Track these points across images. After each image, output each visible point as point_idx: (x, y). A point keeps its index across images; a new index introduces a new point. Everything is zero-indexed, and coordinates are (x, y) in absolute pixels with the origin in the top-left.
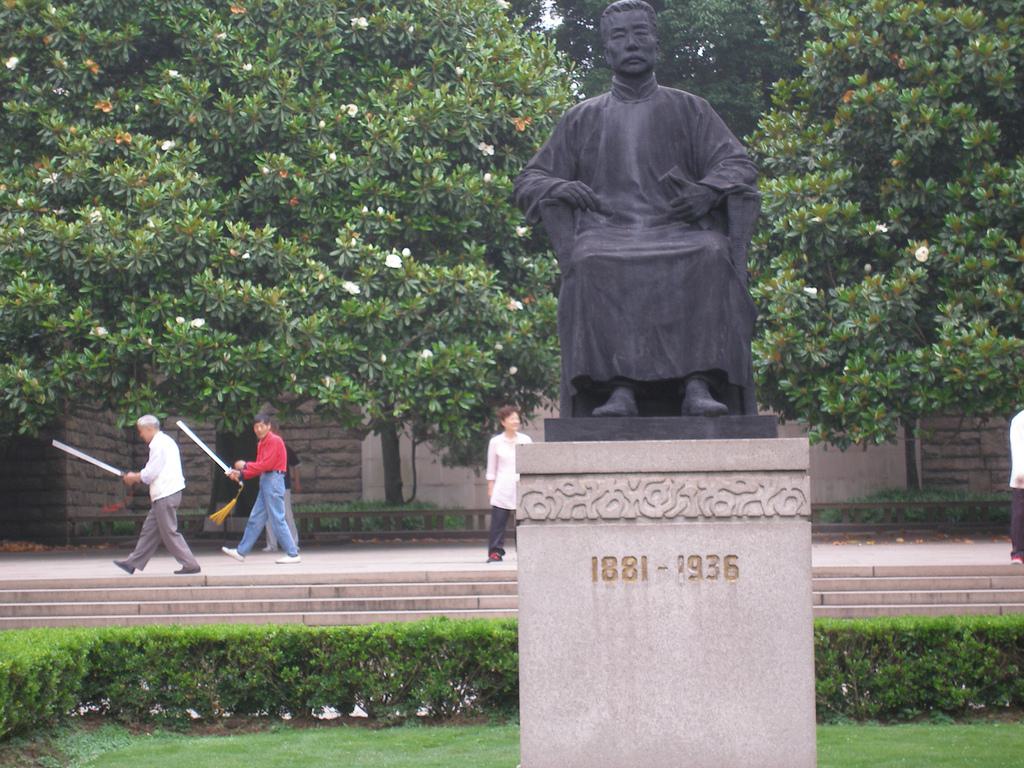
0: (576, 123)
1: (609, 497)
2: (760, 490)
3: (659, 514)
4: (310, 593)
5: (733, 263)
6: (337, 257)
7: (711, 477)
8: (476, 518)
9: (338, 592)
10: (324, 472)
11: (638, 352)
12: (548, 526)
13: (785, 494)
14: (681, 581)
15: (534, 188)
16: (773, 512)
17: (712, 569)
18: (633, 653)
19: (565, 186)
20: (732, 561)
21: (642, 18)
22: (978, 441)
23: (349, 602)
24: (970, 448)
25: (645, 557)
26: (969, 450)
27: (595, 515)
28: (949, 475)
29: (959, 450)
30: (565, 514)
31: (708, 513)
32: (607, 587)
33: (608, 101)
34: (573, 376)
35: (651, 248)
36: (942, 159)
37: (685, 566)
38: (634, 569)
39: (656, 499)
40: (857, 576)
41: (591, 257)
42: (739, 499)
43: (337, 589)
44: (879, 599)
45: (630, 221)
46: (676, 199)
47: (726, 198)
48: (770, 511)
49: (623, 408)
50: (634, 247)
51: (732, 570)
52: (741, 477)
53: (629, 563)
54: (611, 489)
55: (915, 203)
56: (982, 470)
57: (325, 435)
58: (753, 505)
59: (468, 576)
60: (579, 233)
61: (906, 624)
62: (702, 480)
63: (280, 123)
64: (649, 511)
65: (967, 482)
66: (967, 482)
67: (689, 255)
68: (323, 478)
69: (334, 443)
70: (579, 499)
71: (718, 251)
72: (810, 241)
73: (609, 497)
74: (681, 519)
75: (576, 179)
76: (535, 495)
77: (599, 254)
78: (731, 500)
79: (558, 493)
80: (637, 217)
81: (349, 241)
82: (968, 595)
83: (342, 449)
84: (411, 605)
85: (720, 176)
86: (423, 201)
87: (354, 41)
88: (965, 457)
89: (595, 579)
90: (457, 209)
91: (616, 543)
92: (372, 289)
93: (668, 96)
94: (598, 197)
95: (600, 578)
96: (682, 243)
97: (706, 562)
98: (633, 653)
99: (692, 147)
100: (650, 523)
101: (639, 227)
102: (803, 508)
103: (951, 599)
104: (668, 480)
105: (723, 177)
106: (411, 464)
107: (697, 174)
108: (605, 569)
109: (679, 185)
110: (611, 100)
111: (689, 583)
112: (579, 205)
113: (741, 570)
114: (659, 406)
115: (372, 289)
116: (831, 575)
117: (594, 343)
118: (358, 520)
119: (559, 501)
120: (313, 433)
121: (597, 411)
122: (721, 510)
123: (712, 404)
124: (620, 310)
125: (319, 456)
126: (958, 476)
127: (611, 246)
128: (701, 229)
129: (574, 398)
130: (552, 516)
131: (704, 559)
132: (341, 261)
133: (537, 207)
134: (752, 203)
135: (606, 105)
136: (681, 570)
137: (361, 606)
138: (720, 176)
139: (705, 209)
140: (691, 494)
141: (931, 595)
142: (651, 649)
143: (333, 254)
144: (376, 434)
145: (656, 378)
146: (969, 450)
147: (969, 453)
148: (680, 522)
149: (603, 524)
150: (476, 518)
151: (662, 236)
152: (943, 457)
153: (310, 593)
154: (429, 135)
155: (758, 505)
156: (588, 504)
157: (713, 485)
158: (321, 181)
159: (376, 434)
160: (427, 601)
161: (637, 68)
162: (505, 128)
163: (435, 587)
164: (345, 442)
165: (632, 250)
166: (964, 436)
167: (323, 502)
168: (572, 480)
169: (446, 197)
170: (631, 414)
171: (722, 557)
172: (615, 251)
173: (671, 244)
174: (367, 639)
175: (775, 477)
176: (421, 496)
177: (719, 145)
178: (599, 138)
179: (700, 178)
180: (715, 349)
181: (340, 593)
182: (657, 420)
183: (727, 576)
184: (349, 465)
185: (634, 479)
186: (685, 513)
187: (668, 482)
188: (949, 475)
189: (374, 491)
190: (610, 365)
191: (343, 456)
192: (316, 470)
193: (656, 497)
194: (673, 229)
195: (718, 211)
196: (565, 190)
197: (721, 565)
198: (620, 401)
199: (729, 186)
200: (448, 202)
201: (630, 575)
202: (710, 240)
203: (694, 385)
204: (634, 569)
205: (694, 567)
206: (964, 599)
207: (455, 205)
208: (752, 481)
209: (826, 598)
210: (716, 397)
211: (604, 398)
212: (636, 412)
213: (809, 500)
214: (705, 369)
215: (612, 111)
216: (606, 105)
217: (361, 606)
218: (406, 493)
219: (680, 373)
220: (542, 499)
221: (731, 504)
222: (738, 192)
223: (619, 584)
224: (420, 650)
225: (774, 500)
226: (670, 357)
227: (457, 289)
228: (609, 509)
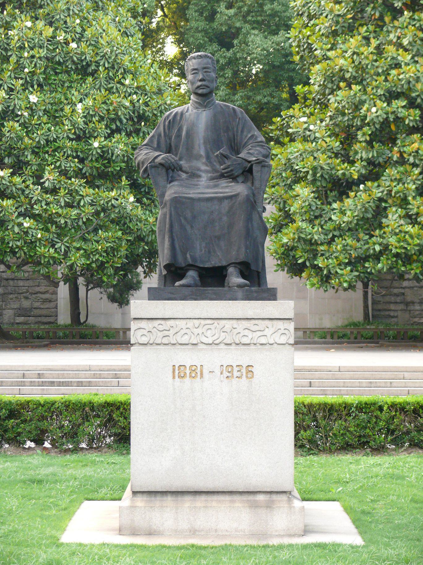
0: (170, 121)
1: (183, 332)
2: (267, 329)
3: (211, 342)
4: (23, 377)
5: (255, 202)
6: (44, 182)
7: (239, 322)
8: (121, 333)
9: (39, 376)
10: (36, 305)
11: (201, 251)
12: (149, 347)
14: (222, 379)
15: (145, 157)
16: (274, 342)
17: (239, 373)
18: (194, 419)
19: (162, 157)
20: (250, 369)
21: (208, 63)
22: (403, 294)
23: (45, 382)
24: (399, 298)
26: (398, 299)
27: (175, 342)
28: (387, 313)
29: (393, 299)
31: (238, 342)
32: (181, 382)
33: (188, 109)
34: (164, 264)
35: (210, 193)
36: (386, 133)
37: (224, 371)
38: (196, 372)
39: (209, 333)
40: (330, 371)
41: (176, 197)
43: (39, 374)
44: (342, 385)
46: (224, 165)
47: (252, 166)
49: (192, 282)
50: (200, 191)
51: (251, 373)
53: (193, 369)
54: (184, 328)
55: (370, 156)
56: (405, 310)
57: (37, 284)
59: (113, 368)
60: (170, 183)
61: (350, 399)
63: (15, 105)
64: (205, 340)
65: (397, 317)
66: (397, 317)
67: (231, 197)
69: (42, 289)
70: (166, 333)
71: (247, 195)
72: (314, 174)
73: (183, 332)
75: (169, 153)
76: (142, 330)
77: (181, 195)
79: (155, 329)
80: (203, 175)
81: (50, 177)
82: (391, 383)
84: (80, 384)
85: (249, 153)
86: (94, 153)
87: (57, 60)
89: (174, 377)
90: (114, 158)
91: (187, 358)
92: (65, 201)
93: (221, 107)
94: (181, 162)
96: (227, 190)
97: (236, 369)
98: (194, 419)
99: (234, 136)
102: (290, 340)
103: (381, 385)
104: (216, 322)
105: (249, 154)
106: (85, 301)
107: (238, 152)
108: (179, 372)
110: (190, 109)
111: (226, 381)
112: (170, 168)
114: (211, 281)
115: (65, 201)
116: (320, 371)
117: (177, 246)
118: (55, 333)
119: (155, 334)
120: (30, 283)
121: (177, 284)
122: (245, 340)
123: (241, 280)
124: (192, 227)
125: (34, 296)
126: (392, 314)
127: (187, 191)
128: (238, 182)
129: (165, 275)
130: (151, 342)
131: (235, 367)
132: (46, 185)
133: (147, 167)
134: (266, 169)
135: (187, 112)
136: (221, 373)
137: (52, 384)
138: (249, 153)
139: (241, 171)
140: (229, 331)
141: (370, 382)
143: (42, 181)
144: (65, 284)
145: (211, 266)
146: (398, 299)
147: (398, 301)
148: (222, 346)
149: (179, 347)
150: (121, 333)
151: (216, 186)
152: (384, 302)
153: (24, 376)
154: (99, 114)
155: (265, 337)
156: (171, 336)
157: (241, 326)
158: (37, 140)
159: (65, 284)
160: (90, 381)
162: (141, 112)
163: (94, 374)
164: (48, 288)
165: (199, 193)
166: (396, 291)
167: (36, 323)
169: (108, 151)
170: (197, 286)
171: (244, 366)
172: (189, 194)
173: (221, 190)
174: (52, 406)
175: (275, 322)
176: (91, 321)
177: (249, 135)
178: (182, 129)
179: (239, 154)
180: (244, 250)
181: (41, 378)
182: (210, 290)
183: (247, 377)
184: (50, 301)
185: (197, 322)
186: (224, 342)
187: (216, 324)
188: (387, 313)
189: (64, 317)
190: (186, 259)
191: (47, 296)
192: (32, 304)
193: (209, 331)
194: (223, 183)
195: (247, 172)
196: (163, 159)
197: (244, 371)
198: (192, 276)
199: (254, 159)
200: (108, 154)
201: (193, 375)
202: (240, 189)
203: (231, 270)
204: (196, 372)
205: (229, 371)
206: (389, 385)
207: (112, 156)
209: (312, 383)
210: (244, 276)
211: (181, 276)
212: (200, 284)
213: (293, 335)
214: (238, 261)
215: (190, 115)
216: (187, 112)
217: (52, 384)
218: (82, 320)
219: (224, 263)
220: (145, 332)
221: (250, 337)
222: (259, 162)
223: (187, 380)
224: (85, 411)
225: (274, 335)
226: (219, 254)
227: (113, 202)
228: (182, 339)
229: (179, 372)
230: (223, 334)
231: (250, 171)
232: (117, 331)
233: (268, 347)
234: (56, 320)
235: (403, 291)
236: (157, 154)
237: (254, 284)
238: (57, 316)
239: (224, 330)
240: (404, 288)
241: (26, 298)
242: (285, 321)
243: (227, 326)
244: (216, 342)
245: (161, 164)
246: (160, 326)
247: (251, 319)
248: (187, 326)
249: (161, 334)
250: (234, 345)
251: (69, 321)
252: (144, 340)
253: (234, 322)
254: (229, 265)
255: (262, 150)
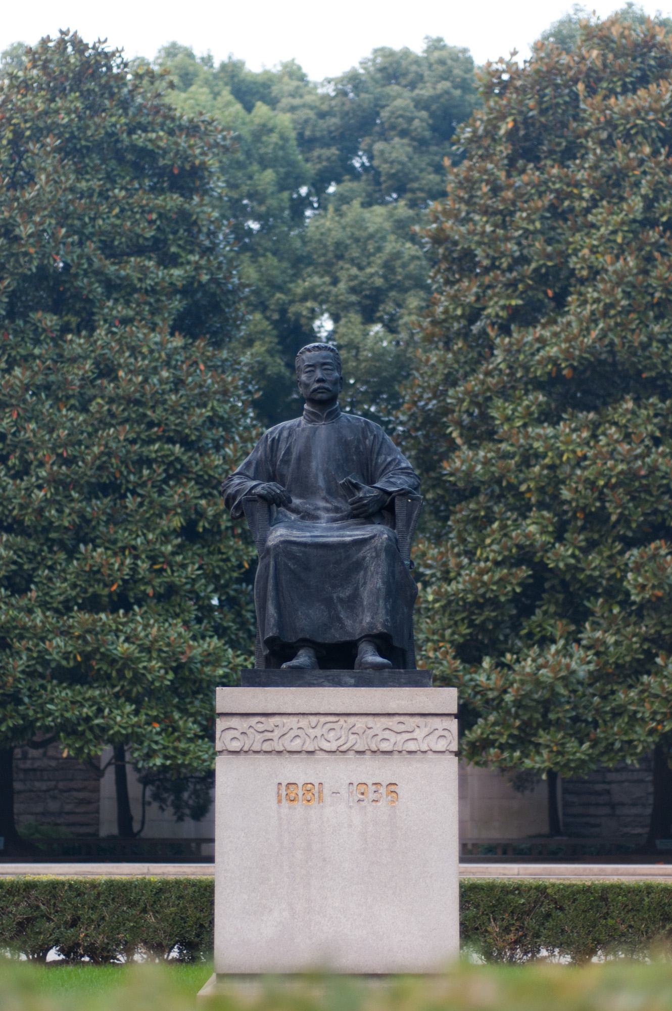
2: (417, 730)
3: (334, 749)
7: (377, 719)
10: (68, 808)
13: (437, 734)
19: (262, 487)
20: (392, 788)
25: (321, 784)
27: (281, 749)
30: (256, 747)
31: (374, 748)
32: (290, 808)
38: (312, 793)
42: (399, 737)
45: (316, 518)
47: (393, 501)
48: (424, 747)
52: (402, 719)
58: (411, 742)
62: (370, 721)
64: (326, 746)
65: (599, 825)
66: (599, 825)
68: (68, 813)
70: (268, 735)
74: (352, 753)
76: (232, 731)
78: (393, 738)
79: (252, 730)
83: (83, 789)
88: (597, 805)
89: (280, 801)
91: (297, 772)
95: (284, 801)
100: (326, 756)
101: (323, 524)
104: (342, 720)
107: (371, 481)
108: (289, 793)
109: (356, 487)
113: (401, 795)
114: (335, 660)
119: (251, 736)
121: (284, 666)
122: (385, 746)
123: (379, 659)
125: (66, 794)
130: (246, 749)
133: (240, 502)
140: (360, 732)
142: (324, 860)
156: (276, 739)
157: (379, 725)
161: (324, 396)
168: (263, 719)
171: (384, 784)
175: (430, 720)
184: (89, 803)
185: (314, 720)
186: (355, 748)
189: (108, 827)
193: (332, 734)
197: (383, 790)
198: (303, 658)
204: (312, 793)
208: (412, 722)
218: (136, 827)
221: (393, 741)
223: (299, 806)
229: (289, 793)
230: (352, 737)
231: (391, 508)
232: (188, 841)
233: (419, 756)
234: (98, 830)
235: (607, 787)
236: (254, 483)
237: (398, 660)
238: (98, 824)
239: (354, 730)
240: (609, 783)
241: (54, 798)
242: (444, 718)
243: (358, 725)
244: (342, 749)
245: (261, 496)
246: (260, 725)
247: (394, 714)
248: (300, 725)
249: (260, 737)
250: (368, 753)
251: (115, 831)
252: (235, 746)
253: (370, 719)
254: (360, 639)
255: (407, 479)
